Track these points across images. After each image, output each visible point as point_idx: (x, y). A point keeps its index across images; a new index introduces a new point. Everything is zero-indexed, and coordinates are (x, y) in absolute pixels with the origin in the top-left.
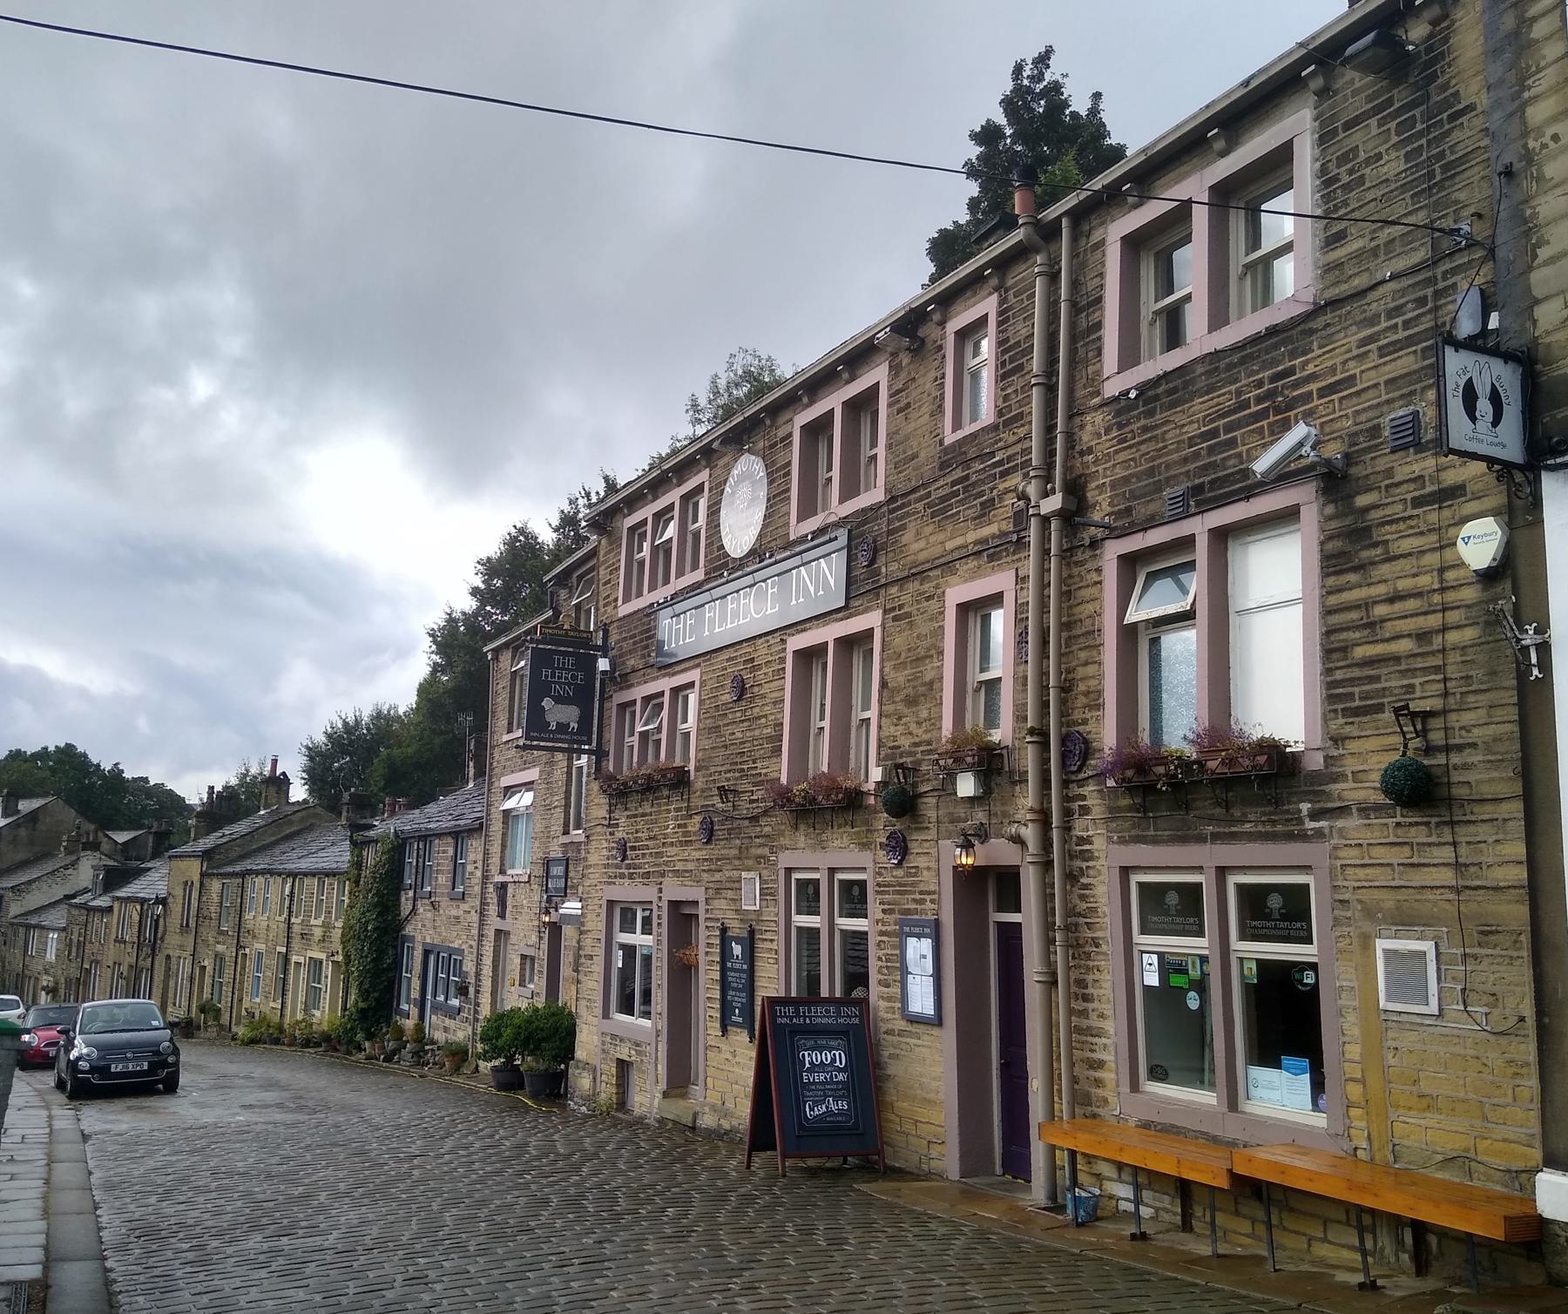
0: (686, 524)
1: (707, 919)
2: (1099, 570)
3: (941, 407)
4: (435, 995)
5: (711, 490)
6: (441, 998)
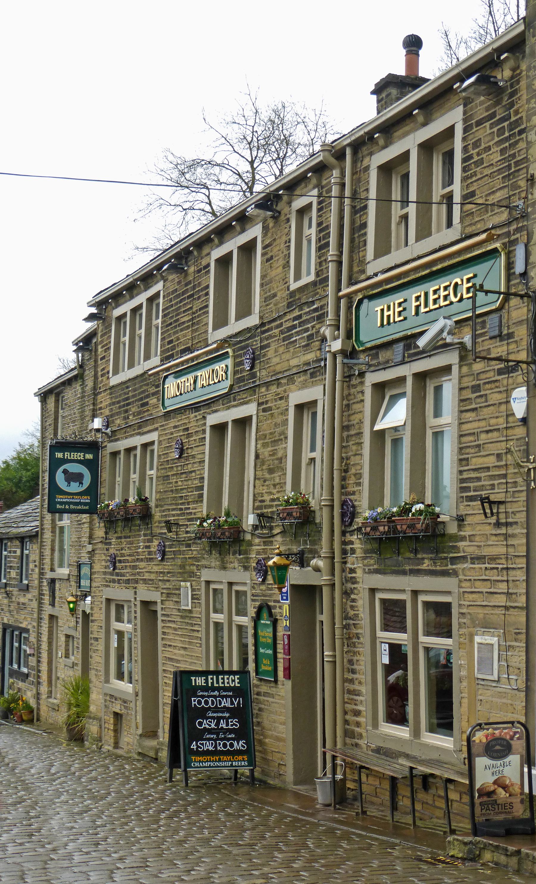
0: (151, 319)
1: (163, 615)
2: (362, 392)
3: (288, 262)
4: (11, 663)
5: (164, 297)
6: (15, 666)
